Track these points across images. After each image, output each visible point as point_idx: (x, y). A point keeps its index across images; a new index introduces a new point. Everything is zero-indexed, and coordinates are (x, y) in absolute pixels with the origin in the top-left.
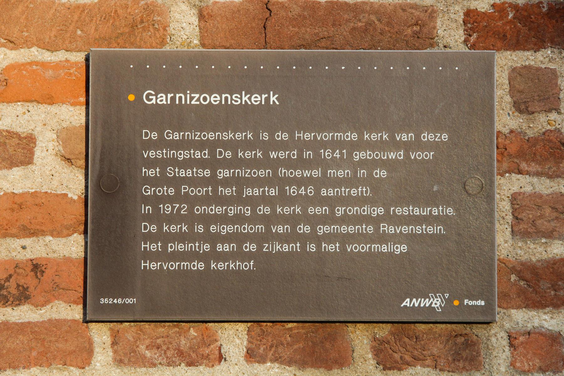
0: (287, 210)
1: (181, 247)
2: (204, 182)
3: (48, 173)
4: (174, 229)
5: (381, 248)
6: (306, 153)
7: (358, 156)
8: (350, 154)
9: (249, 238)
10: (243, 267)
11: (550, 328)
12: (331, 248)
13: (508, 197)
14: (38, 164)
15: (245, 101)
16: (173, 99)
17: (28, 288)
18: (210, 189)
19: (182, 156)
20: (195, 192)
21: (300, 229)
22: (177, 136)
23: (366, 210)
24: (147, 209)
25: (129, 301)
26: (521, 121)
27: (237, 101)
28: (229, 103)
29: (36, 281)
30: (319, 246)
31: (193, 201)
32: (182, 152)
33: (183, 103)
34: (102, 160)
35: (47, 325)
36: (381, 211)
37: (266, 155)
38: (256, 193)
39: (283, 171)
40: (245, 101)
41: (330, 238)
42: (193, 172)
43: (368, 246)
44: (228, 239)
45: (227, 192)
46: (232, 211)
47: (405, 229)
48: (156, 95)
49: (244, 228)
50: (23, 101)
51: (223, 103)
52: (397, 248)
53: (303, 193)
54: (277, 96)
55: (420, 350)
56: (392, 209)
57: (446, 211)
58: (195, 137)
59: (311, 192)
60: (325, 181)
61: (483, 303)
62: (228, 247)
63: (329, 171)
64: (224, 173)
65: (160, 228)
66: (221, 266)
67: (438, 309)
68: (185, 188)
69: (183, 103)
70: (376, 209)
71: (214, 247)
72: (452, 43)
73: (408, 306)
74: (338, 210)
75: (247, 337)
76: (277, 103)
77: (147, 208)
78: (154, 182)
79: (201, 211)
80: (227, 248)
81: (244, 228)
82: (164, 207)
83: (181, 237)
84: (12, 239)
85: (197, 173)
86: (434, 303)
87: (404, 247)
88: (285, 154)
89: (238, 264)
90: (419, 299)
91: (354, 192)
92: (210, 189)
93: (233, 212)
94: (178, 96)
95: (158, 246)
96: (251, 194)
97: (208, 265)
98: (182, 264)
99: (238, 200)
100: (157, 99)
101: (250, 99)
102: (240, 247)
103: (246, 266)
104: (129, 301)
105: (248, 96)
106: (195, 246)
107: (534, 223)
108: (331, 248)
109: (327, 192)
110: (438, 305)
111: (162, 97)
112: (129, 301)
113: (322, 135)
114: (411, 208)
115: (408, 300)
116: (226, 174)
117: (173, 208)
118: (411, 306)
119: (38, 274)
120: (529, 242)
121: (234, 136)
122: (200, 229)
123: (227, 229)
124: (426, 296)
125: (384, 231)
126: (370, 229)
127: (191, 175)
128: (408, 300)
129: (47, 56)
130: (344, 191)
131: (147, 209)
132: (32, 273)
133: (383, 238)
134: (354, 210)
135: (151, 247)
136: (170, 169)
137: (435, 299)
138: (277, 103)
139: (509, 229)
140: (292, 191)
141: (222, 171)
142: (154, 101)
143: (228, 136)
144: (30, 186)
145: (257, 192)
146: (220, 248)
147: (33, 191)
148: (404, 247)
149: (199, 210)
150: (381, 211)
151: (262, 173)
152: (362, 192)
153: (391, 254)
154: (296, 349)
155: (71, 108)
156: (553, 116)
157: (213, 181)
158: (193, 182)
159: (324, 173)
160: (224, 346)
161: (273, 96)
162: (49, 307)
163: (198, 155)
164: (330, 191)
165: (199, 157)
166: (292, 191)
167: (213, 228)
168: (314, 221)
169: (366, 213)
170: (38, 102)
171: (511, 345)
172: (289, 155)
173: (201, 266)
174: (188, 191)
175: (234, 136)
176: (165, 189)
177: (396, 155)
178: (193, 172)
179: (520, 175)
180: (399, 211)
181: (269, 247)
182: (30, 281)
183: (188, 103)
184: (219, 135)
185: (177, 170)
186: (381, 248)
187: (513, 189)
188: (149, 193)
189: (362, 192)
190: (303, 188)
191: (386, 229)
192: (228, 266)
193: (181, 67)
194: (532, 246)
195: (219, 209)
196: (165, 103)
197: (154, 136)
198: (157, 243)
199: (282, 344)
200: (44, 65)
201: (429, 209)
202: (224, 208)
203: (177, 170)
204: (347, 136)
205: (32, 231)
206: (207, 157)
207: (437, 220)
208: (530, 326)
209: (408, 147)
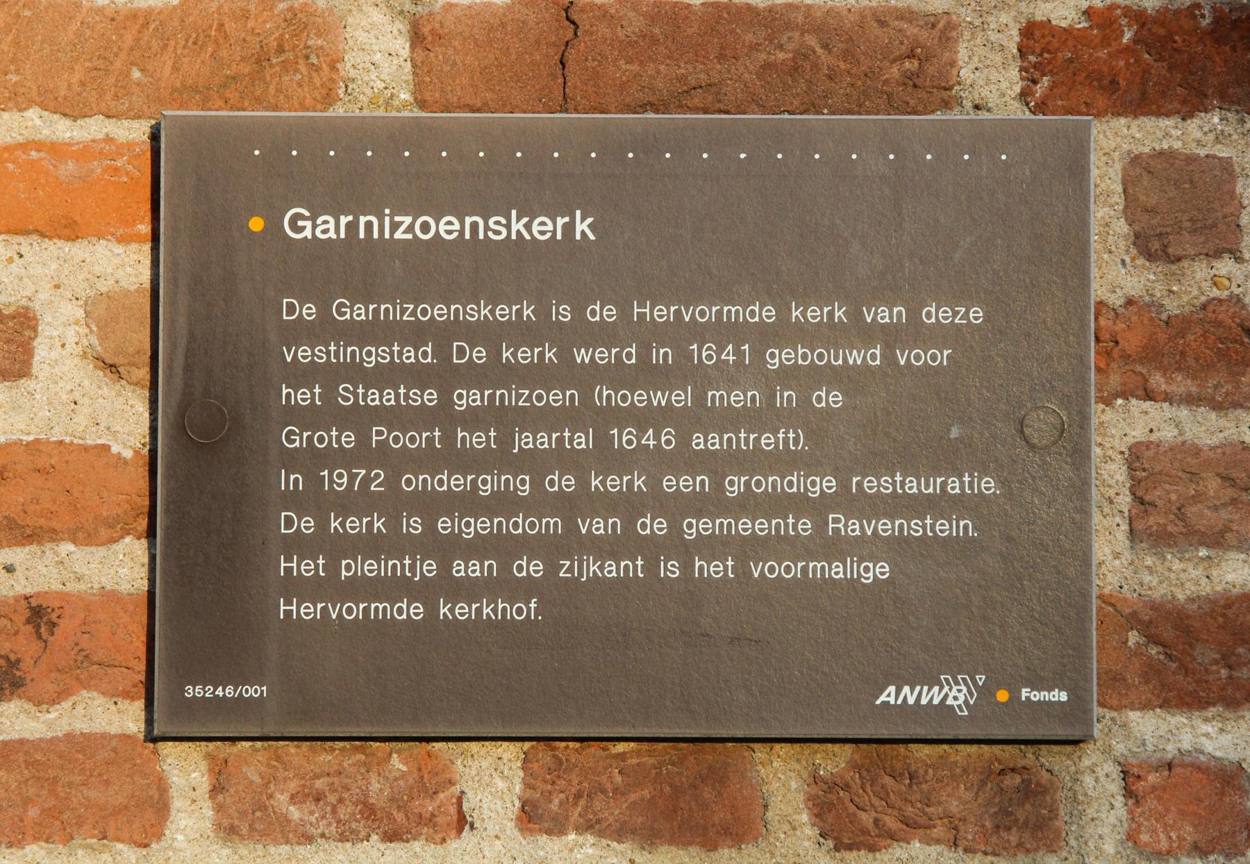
0: (615, 483)
1: (370, 568)
3: (64, 396)
4: (354, 525)
5: (830, 569)
6: (658, 353)
7: (777, 358)
8: (758, 354)
9: (526, 546)
10: (512, 613)
12: (715, 569)
13: (1122, 453)
16: (352, 227)
17: (18, 661)
18: (437, 434)
19: (373, 358)
21: (644, 525)
22: (360, 313)
23: (795, 483)
24: (293, 480)
26: (1152, 277)
28: (481, 236)
29: (36, 646)
30: (687, 566)
32: (373, 350)
33: (376, 236)
34: (188, 368)
35: (62, 747)
36: (829, 484)
39: (605, 393)
40: (518, 232)
41: (712, 547)
42: (397, 396)
43: (800, 565)
45: (477, 440)
46: (488, 485)
47: (885, 527)
48: (313, 219)
51: (467, 236)
52: (867, 569)
53: (652, 443)
54: (590, 220)
55: (919, 805)
56: (855, 480)
57: (979, 485)
58: (402, 314)
59: (668, 442)
60: (701, 417)
61: (1064, 697)
63: (710, 394)
65: (323, 524)
66: (463, 611)
67: (961, 710)
68: (379, 433)
69: (376, 236)
70: (818, 480)
71: (445, 567)
72: (993, 100)
73: (892, 702)
74: (732, 483)
76: (592, 237)
77: (292, 477)
78: (309, 418)
80: (475, 569)
81: (516, 525)
82: (330, 475)
83: (371, 546)
85: (407, 397)
88: (610, 353)
89: (500, 607)
90: (918, 688)
92: (437, 434)
93: (489, 486)
96: (531, 446)
97: (432, 610)
98: (373, 606)
99: (502, 459)
100: (314, 227)
101: (528, 226)
102: (505, 568)
105: (525, 220)
106: (403, 566)
108: (715, 569)
109: (706, 441)
110: (961, 702)
111: (326, 222)
112: (252, 691)
113: (694, 310)
115: (892, 689)
116: (474, 401)
117: (352, 477)
119: (43, 630)
120: (1169, 557)
121: (492, 312)
122: (414, 525)
124: (933, 681)
126: (805, 526)
127: (393, 402)
128: (892, 689)
129: (63, 130)
130: (744, 439)
131: (293, 480)
132: (29, 628)
133: (835, 548)
134: (768, 483)
136: (346, 389)
137: (955, 688)
138: (592, 237)
140: (624, 439)
141: (464, 392)
142: (308, 233)
145: (544, 441)
146: (459, 569)
147: (31, 438)
149: (412, 482)
150: (829, 484)
151: (556, 398)
152: (786, 440)
153: (852, 584)
154: (634, 803)
155: (119, 249)
156: (1225, 266)
157: (443, 415)
158: (397, 418)
159: (700, 398)
160: (470, 794)
162: (66, 705)
163: (410, 356)
165: (412, 360)
166: (625, 438)
167: (444, 525)
169: (795, 489)
170: (43, 235)
171: (1129, 793)
172: (618, 355)
173: (416, 611)
175: (492, 312)
178: (397, 396)
179: (1149, 403)
180: (871, 485)
181: (572, 566)
183: (387, 236)
184: (457, 310)
185: (361, 391)
186: (830, 569)
187: (1134, 433)
189: (786, 440)
191: (840, 526)
192: (479, 611)
194: (1177, 565)
196: (334, 237)
197: (309, 312)
198: (315, 560)
199: (604, 791)
200: (56, 149)
202: (469, 478)
203: (361, 391)
204: (753, 312)
205: (28, 532)
206: (429, 360)
209: (891, 337)
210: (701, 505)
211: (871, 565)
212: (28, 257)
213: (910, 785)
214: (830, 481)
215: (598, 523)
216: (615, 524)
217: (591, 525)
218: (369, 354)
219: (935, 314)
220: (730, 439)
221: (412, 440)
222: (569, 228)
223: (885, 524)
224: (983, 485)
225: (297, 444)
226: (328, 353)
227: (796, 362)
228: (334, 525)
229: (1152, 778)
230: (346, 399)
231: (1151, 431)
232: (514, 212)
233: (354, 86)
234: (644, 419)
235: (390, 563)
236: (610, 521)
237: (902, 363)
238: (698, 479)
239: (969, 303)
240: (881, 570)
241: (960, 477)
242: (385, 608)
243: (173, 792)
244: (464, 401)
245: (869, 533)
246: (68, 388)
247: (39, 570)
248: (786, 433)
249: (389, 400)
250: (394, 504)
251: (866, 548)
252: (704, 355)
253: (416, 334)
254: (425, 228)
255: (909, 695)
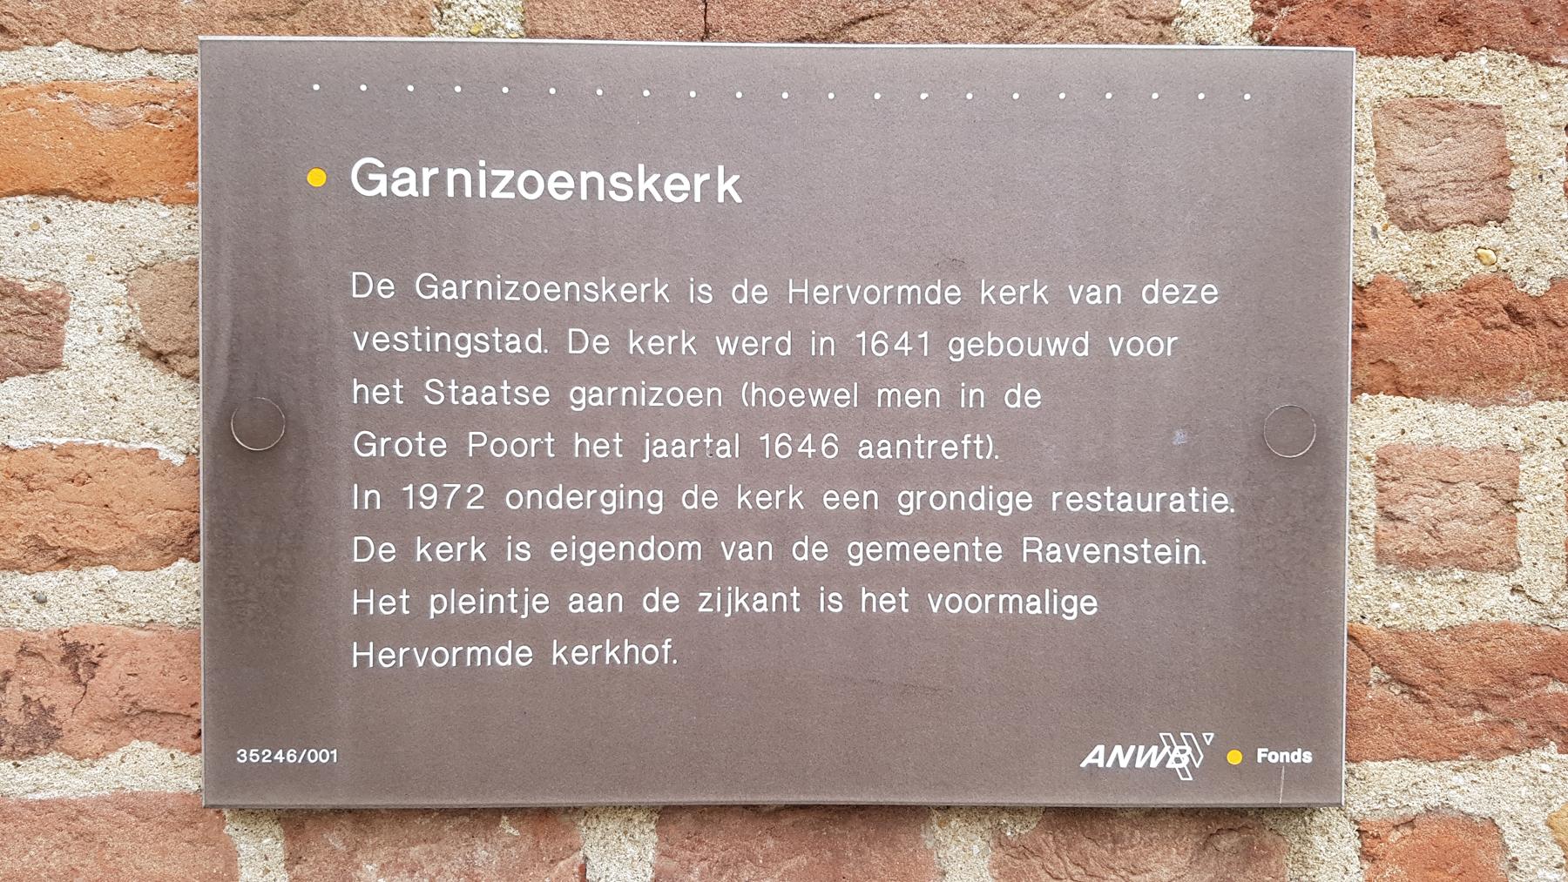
0: (765, 500)
1: (464, 604)
2: (530, 421)
3: (102, 392)
4: (446, 552)
5: (1025, 603)
6: (818, 342)
7: (962, 349)
8: (940, 345)
9: (661, 576)
10: (640, 656)
11: (1469, 810)
12: (887, 603)
13: (1368, 459)
14: (74, 369)
15: (647, 191)
16: (438, 182)
17: (52, 709)
18: (549, 440)
19: (468, 347)
20: (507, 448)
21: (800, 549)
22: (451, 291)
23: (982, 500)
24: (365, 497)
25: (318, 756)
26: (1406, 248)
27: (623, 193)
28: (601, 197)
29: (72, 692)
30: (852, 599)
31: (498, 476)
32: (468, 337)
33: (468, 193)
34: (233, 359)
35: (108, 810)
36: (1023, 501)
37: (705, 344)
38: (678, 452)
39: (754, 392)
40: (647, 191)
41: (882, 576)
42: (499, 394)
43: (988, 598)
44: (599, 578)
45: (597, 448)
46: (613, 502)
47: (1093, 553)
48: (388, 171)
49: (646, 548)
50: (31, 192)
51: (584, 196)
52: (1069, 603)
53: (810, 451)
54: (735, 178)
55: (1123, 873)
56: (1055, 496)
57: (1209, 502)
58: (504, 292)
59: (830, 450)
60: (870, 418)
61: (1308, 757)
62: (600, 602)
63: (880, 392)
64: (587, 395)
65: (406, 550)
66: (581, 655)
67: (1185, 775)
68: (477, 439)
69: (468, 193)
70: (1010, 495)
71: (559, 601)
72: (1222, 33)
73: (1101, 765)
74: (906, 499)
75: (655, 837)
76: (738, 199)
77: (367, 494)
78: (387, 421)
79: (525, 503)
80: (597, 604)
81: (646, 549)
82: (415, 490)
83: (468, 577)
84: (9, 574)
85: (511, 394)
86: (1172, 760)
87: (1089, 601)
88: (760, 342)
89: (627, 649)
90: (1132, 748)
91: (949, 449)
92: (549, 440)
93: (613, 504)
94: (451, 173)
95: (399, 602)
96: (664, 454)
97: (543, 653)
98: (469, 650)
99: (631, 471)
100: (390, 181)
101: (659, 185)
102: (633, 601)
103: (650, 654)
104: (318, 756)
105: (655, 177)
106: (507, 601)
107: (1434, 532)
108: (887, 603)
109: (875, 449)
110: (1184, 764)
111: (405, 176)
112: (319, 756)
113: (862, 290)
114: (1109, 494)
115: (1100, 749)
116: (595, 400)
117: (443, 493)
118: (1109, 764)
119: (81, 671)
120: (1419, 580)
121: (616, 291)
122: (521, 551)
123: (595, 552)
124: (1151, 740)
125: (1033, 556)
126: (994, 552)
127: (494, 402)
128: (1100, 749)
129: (95, 66)
130: (921, 446)
131: (365, 497)
132: (65, 669)
133: (1033, 577)
134: (947, 500)
135: (381, 604)
136: (433, 385)
137: (1177, 748)
138: (738, 199)
139: (1369, 547)
140: (777, 446)
141: (583, 390)
142: (382, 189)
143: (599, 291)
144: (53, 428)
145: (681, 449)
146: (577, 604)
147: (64, 440)
148: (1089, 601)
149: (519, 499)
150: (1023, 501)
151: (695, 396)
152: (972, 447)
153: (1054, 621)
154: (788, 872)
155: (164, 212)
156: (1492, 234)
157: (557, 418)
158: (496, 420)
159: (867, 398)
160: (593, 860)
161: (726, 179)
162: (115, 757)
163: (514, 344)
164: (884, 445)
165: (518, 350)
166: (777, 445)
167: (557, 551)
168: (838, 529)
169: (982, 507)
170: (74, 196)
171: (1365, 855)
172: (770, 347)
173: (523, 656)
174: (488, 444)
175: (616, 291)
176: (420, 439)
177: (1070, 346)
178: (499, 394)
179: (1399, 398)
180: (1075, 501)
181: (713, 600)
182: (59, 693)
183: (483, 194)
184: (572, 288)
185: (453, 387)
186: (1025, 603)
187: (1383, 435)
188: (373, 452)
189: (972, 447)
190: (809, 437)
191: (1037, 550)
192: (600, 654)
193: (458, 89)
194: (1427, 590)
195: (574, 495)
196: (416, 194)
197: (384, 288)
198: (396, 594)
199: (753, 859)
200: (88, 95)
201: (1159, 496)
202: (589, 494)
203: (453, 387)
204: (933, 292)
205: (60, 553)
206: (539, 350)
207: (1186, 527)
208: (1417, 806)
209: (1108, 322)
210: (871, 525)
211: (1075, 599)
212: (58, 222)
213: (1114, 851)
214: (1024, 497)
215: (745, 547)
216: (765, 548)
217: (737, 549)
218: (463, 341)
219: (1158, 293)
220: (904, 446)
221: (519, 446)
222: (709, 188)
223: (1092, 549)
224: (1214, 503)
225: (373, 452)
226: (411, 340)
227: (985, 354)
228: (420, 551)
229: (1395, 836)
230: (435, 397)
231: (1403, 432)
232: (641, 168)
233: (450, 12)
234: (800, 421)
235: (491, 598)
236: (760, 545)
237: (1116, 353)
238: (866, 494)
239: (1202, 276)
240: (1082, 606)
241: (1186, 492)
242: (485, 652)
243: (242, 861)
244: (583, 401)
245: (1072, 560)
246: (106, 381)
247: (72, 601)
248: (972, 438)
249: (488, 399)
250: (494, 525)
251: (1073, 578)
252: (874, 344)
253: (521, 317)
254: (531, 184)
255: (1121, 757)
